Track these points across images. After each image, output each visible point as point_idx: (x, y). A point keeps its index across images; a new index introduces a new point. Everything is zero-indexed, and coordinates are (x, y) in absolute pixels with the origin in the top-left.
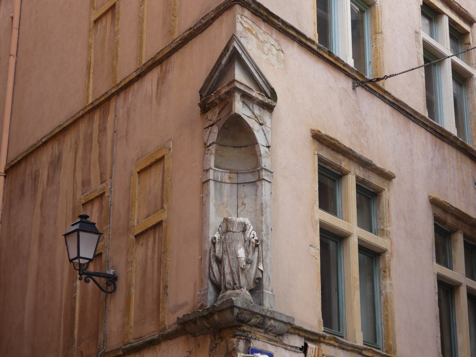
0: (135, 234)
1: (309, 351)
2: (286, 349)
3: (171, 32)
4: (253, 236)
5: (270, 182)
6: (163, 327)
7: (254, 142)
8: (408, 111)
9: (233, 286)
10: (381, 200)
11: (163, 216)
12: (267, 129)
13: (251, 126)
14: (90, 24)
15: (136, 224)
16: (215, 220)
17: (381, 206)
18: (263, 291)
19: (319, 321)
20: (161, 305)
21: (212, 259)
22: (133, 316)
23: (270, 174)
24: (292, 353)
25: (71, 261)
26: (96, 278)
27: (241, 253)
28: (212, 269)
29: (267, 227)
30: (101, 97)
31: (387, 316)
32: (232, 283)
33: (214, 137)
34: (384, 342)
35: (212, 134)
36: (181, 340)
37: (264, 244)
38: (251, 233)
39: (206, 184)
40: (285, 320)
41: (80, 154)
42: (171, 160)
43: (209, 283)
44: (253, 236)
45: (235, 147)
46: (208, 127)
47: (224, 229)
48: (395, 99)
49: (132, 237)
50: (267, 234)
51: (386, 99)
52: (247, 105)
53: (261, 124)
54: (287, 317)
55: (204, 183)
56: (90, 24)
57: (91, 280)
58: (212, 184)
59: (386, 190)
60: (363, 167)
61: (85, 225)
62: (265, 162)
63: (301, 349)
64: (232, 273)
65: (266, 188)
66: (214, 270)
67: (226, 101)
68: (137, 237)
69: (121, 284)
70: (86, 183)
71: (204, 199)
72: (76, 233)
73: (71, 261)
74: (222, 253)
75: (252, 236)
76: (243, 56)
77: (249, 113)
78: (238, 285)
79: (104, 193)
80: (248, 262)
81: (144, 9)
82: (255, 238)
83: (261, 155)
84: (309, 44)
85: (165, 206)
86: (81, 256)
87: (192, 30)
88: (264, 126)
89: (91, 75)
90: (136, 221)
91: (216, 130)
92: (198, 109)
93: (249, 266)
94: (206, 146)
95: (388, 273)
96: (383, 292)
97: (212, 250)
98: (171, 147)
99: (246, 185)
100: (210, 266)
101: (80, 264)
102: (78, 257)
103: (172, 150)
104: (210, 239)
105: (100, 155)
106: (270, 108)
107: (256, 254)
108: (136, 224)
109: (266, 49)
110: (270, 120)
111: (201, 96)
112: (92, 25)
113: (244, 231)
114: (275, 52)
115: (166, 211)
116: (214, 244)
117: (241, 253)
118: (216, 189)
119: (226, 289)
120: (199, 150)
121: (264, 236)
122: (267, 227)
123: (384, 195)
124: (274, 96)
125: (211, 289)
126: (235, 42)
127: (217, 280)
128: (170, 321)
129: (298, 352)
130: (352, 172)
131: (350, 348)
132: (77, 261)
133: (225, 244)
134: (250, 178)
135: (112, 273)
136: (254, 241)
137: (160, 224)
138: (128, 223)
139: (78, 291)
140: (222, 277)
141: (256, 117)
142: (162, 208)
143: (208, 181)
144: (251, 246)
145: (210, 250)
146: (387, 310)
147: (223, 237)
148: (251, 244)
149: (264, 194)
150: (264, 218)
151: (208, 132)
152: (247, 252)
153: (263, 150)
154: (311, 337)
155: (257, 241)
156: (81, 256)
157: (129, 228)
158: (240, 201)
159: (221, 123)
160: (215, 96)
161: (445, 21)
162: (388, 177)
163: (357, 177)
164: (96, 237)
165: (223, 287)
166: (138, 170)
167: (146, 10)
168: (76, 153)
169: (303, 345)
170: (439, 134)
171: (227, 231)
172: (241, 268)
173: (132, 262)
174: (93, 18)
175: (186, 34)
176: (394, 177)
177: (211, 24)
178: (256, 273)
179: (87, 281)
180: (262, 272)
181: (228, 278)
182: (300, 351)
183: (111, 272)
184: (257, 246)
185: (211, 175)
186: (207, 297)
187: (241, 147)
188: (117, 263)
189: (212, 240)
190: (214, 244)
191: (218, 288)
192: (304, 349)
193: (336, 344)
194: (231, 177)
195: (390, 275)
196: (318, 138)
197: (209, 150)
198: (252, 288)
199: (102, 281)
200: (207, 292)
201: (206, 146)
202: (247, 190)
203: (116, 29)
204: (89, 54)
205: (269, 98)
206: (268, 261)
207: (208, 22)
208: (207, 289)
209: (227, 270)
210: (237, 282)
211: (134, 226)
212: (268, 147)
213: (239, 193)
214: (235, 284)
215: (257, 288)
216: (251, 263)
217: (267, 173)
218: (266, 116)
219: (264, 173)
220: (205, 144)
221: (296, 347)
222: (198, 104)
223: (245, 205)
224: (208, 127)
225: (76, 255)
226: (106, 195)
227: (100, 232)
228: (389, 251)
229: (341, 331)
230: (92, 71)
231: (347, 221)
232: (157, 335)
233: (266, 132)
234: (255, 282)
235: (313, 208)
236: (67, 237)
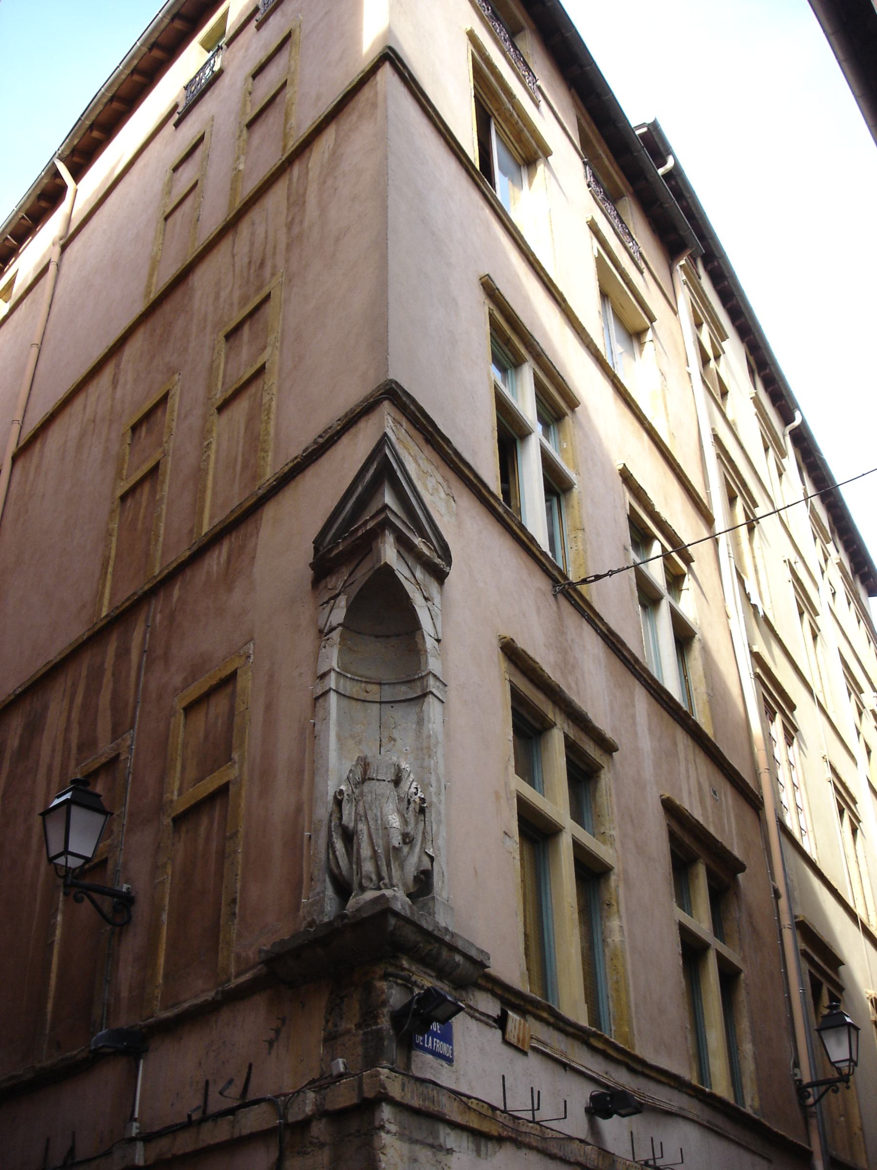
0: (173, 815)
1: (510, 1025)
2: (472, 1017)
3: (255, 477)
4: (415, 790)
5: (443, 702)
6: (225, 977)
7: (415, 625)
8: (625, 653)
9: (376, 882)
10: (599, 786)
11: (232, 774)
12: (436, 610)
13: (411, 595)
14: (113, 503)
15: (175, 798)
16: (336, 769)
17: (598, 795)
18: (433, 898)
19: (522, 974)
20: (221, 936)
21: (334, 833)
22: (162, 967)
23: (441, 686)
24: (482, 1026)
25: (51, 860)
26: (95, 896)
27: (395, 821)
28: (334, 852)
29: (438, 780)
30: (123, 603)
31: (617, 982)
32: (374, 877)
33: (339, 615)
34: (613, 1028)
35: (334, 612)
36: (260, 1001)
37: (433, 810)
38: (410, 785)
39: (321, 700)
40: (473, 953)
41: (79, 700)
42: (250, 674)
43: (328, 880)
44: (415, 790)
45: (377, 637)
46: (327, 602)
47: (358, 776)
48: (609, 629)
49: (167, 821)
50: (439, 794)
51: (597, 626)
52: (404, 559)
53: (426, 599)
54: (478, 949)
55: (317, 699)
56: (113, 503)
57: (86, 899)
58: (333, 697)
59: (606, 768)
60: (573, 721)
61: (84, 794)
62: (433, 664)
63: (495, 1020)
64: (375, 856)
65: (432, 707)
66: (337, 853)
67: (366, 545)
68: (178, 820)
69: (141, 910)
70: (88, 744)
71: (317, 727)
72: (65, 807)
73: (51, 860)
74: (356, 821)
75: (413, 790)
76: (399, 474)
77: (407, 574)
78: (387, 881)
79: (118, 755)
80: (407, 839)
81: (209, 456)
82: (419, 795)
83: (426, 651)
84: (492, 501)
85: (235, 756)
86: (71, 849)
87: (298, 460)
88: (430, 603)
89: (109, 577)
90: (176, 793)
91: (342, 601)
92: (310, 572)
93: (406, 849)
94: (323, 633)
95: (615, 908)
96: (609, 940)
97: (336, 816)
98: (251, 652)
99: (396, 705)
100: (330, 845)
101: (67, 869)
102: (66, 852)
103: (252, 657)
104: (330, 798)
105: (115, 694)
106: (440, 576)
107: (421, 825)
108: (175, 798)
109: (430, 486)
110: (439, 597)
111: (316, 550)
112: (116, 503)
113: (397, 782)
114: (443, 495)
115: (237, 766)
116: (338, 803)
117: (395, 821)
118: (339, 709)
119: (363, 889)
120: (307, 641)
121: (433, 795)
122: (438, 780)
123: (602, 776)
124: (445, 553)
125: (330, 892)
126: (386, 448)
127: (344, 872)
128: (248, 943)
129: (492, 1027)
130: (558, 726)
131: (571, 1030)
132: (61, 861)
133: (361, 803)
134: (404, 692)
135: (124, 890)
136: (417, 800)
137: (223, 790)
138: (161, 795)
139: (58, 932)
140: (354, 867)
141: (418, 584)
142: (230, 759)
143: (325, 693)
144: (411, 809)
145: (331, 815)
146: (618, 973)
147: (357, 791)
148: (412, 805)
149: (432, 720)
150: (432, 762)
151: (328, 610)
152: (405, 822)
153: (430, 643)
154: (513, 999)
155: (423, 800)
156: (71, 849)
157: (160, 807)
158: (386, 734)
159: (355, 589)
160: (342, 549)
161: (656, 549)
162: (608, 747)
163: (566, 737)
164: (99, 819)
165: (355, 886)
166: (185, 703)
167: (213, 457)
168: (72, 702)
169: (499, 1013)
170: (666, 703)
171: (365, 779)
172: (394, 847)
173: (164, 865)
174: (119, 493)
175: (287, 469)
176: (616, 750)
177: (336, 441)
178: (420, 860)
179: (79, 900)
180: (432, 859)
181: (368, 867)
182: (494, 1024)
183: (125, 888)
184: (422, 811)
185: (332, 681)
186: (322, 906)
187: (388, 637)
188: (136, 874)
189: (335, 797)
190: (338, 803)
191: (343, 889)
192: (501, 1022)
193: (552, 1020)
194: (368, 690)
195: (618, 911)
196: (511, 652)
197: (328, 639)
198: (412, 890)
199: (107, 904)
200: (324, 896)
201: (323, 633)
202: (397, 713)
203: (158, 497)
204: (108, 547)
205: (439, 557)
206: (441, 842)
207: (332, 437)
208: (323, 892)
209: (366, 852)
210: (385, 874)
211: (172, 801)
212: (438, 641)
213: (383, 720)
214: (380, 878)
215: (423, 883)
216: (411, 842)
217: (438, 683)
218: (433, 588)
219: (431, 681)
220: (321, 631)
221: (489, 1016)
222: (310, 564)
223: (394, 740)
224: (327, 602)
225: (61, 849)
226: (122, 757)
227: (108, 809)
228: (616, 870)
229: (550, 1000)
230: (110, 569)
231: (556, 804)
232: (213, 994)
233: (433, 613)
234: (416, 879)
235: (506, 768)
236: (47, 816)
